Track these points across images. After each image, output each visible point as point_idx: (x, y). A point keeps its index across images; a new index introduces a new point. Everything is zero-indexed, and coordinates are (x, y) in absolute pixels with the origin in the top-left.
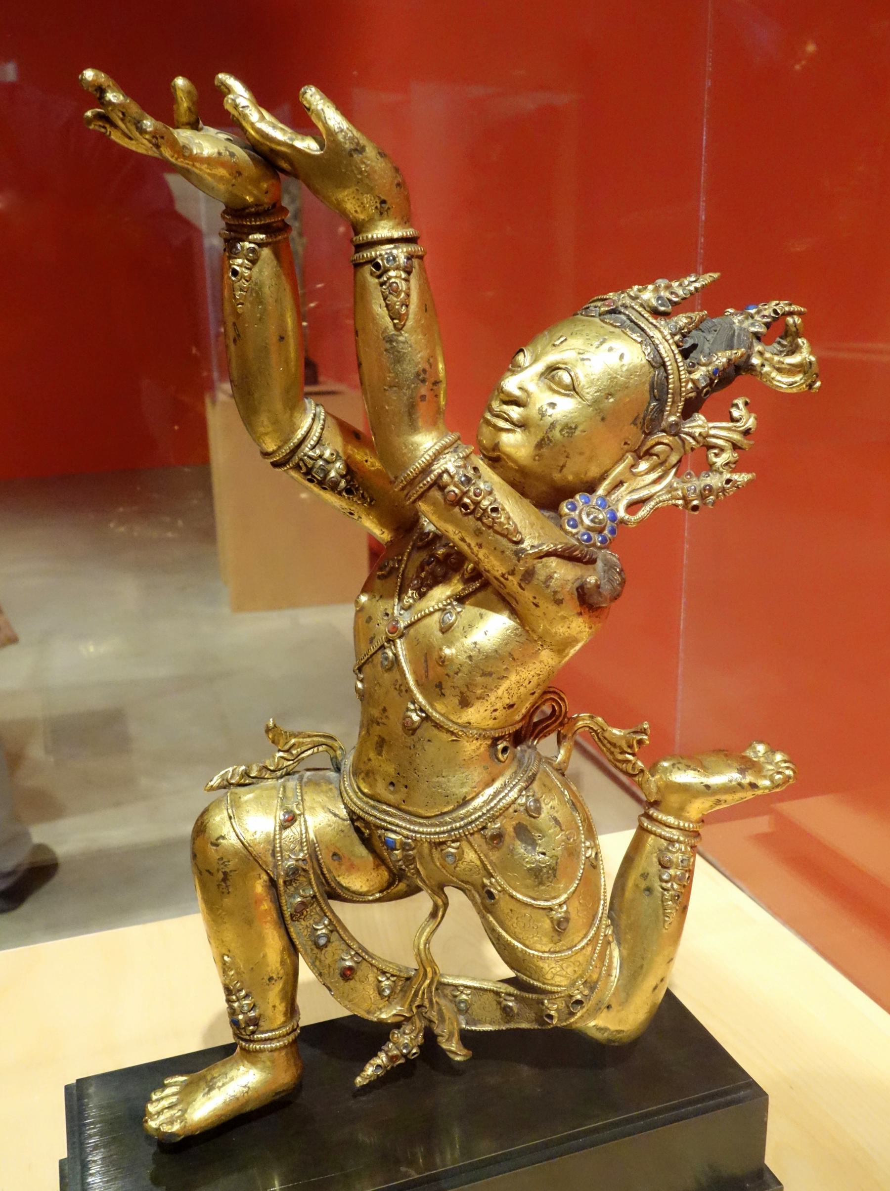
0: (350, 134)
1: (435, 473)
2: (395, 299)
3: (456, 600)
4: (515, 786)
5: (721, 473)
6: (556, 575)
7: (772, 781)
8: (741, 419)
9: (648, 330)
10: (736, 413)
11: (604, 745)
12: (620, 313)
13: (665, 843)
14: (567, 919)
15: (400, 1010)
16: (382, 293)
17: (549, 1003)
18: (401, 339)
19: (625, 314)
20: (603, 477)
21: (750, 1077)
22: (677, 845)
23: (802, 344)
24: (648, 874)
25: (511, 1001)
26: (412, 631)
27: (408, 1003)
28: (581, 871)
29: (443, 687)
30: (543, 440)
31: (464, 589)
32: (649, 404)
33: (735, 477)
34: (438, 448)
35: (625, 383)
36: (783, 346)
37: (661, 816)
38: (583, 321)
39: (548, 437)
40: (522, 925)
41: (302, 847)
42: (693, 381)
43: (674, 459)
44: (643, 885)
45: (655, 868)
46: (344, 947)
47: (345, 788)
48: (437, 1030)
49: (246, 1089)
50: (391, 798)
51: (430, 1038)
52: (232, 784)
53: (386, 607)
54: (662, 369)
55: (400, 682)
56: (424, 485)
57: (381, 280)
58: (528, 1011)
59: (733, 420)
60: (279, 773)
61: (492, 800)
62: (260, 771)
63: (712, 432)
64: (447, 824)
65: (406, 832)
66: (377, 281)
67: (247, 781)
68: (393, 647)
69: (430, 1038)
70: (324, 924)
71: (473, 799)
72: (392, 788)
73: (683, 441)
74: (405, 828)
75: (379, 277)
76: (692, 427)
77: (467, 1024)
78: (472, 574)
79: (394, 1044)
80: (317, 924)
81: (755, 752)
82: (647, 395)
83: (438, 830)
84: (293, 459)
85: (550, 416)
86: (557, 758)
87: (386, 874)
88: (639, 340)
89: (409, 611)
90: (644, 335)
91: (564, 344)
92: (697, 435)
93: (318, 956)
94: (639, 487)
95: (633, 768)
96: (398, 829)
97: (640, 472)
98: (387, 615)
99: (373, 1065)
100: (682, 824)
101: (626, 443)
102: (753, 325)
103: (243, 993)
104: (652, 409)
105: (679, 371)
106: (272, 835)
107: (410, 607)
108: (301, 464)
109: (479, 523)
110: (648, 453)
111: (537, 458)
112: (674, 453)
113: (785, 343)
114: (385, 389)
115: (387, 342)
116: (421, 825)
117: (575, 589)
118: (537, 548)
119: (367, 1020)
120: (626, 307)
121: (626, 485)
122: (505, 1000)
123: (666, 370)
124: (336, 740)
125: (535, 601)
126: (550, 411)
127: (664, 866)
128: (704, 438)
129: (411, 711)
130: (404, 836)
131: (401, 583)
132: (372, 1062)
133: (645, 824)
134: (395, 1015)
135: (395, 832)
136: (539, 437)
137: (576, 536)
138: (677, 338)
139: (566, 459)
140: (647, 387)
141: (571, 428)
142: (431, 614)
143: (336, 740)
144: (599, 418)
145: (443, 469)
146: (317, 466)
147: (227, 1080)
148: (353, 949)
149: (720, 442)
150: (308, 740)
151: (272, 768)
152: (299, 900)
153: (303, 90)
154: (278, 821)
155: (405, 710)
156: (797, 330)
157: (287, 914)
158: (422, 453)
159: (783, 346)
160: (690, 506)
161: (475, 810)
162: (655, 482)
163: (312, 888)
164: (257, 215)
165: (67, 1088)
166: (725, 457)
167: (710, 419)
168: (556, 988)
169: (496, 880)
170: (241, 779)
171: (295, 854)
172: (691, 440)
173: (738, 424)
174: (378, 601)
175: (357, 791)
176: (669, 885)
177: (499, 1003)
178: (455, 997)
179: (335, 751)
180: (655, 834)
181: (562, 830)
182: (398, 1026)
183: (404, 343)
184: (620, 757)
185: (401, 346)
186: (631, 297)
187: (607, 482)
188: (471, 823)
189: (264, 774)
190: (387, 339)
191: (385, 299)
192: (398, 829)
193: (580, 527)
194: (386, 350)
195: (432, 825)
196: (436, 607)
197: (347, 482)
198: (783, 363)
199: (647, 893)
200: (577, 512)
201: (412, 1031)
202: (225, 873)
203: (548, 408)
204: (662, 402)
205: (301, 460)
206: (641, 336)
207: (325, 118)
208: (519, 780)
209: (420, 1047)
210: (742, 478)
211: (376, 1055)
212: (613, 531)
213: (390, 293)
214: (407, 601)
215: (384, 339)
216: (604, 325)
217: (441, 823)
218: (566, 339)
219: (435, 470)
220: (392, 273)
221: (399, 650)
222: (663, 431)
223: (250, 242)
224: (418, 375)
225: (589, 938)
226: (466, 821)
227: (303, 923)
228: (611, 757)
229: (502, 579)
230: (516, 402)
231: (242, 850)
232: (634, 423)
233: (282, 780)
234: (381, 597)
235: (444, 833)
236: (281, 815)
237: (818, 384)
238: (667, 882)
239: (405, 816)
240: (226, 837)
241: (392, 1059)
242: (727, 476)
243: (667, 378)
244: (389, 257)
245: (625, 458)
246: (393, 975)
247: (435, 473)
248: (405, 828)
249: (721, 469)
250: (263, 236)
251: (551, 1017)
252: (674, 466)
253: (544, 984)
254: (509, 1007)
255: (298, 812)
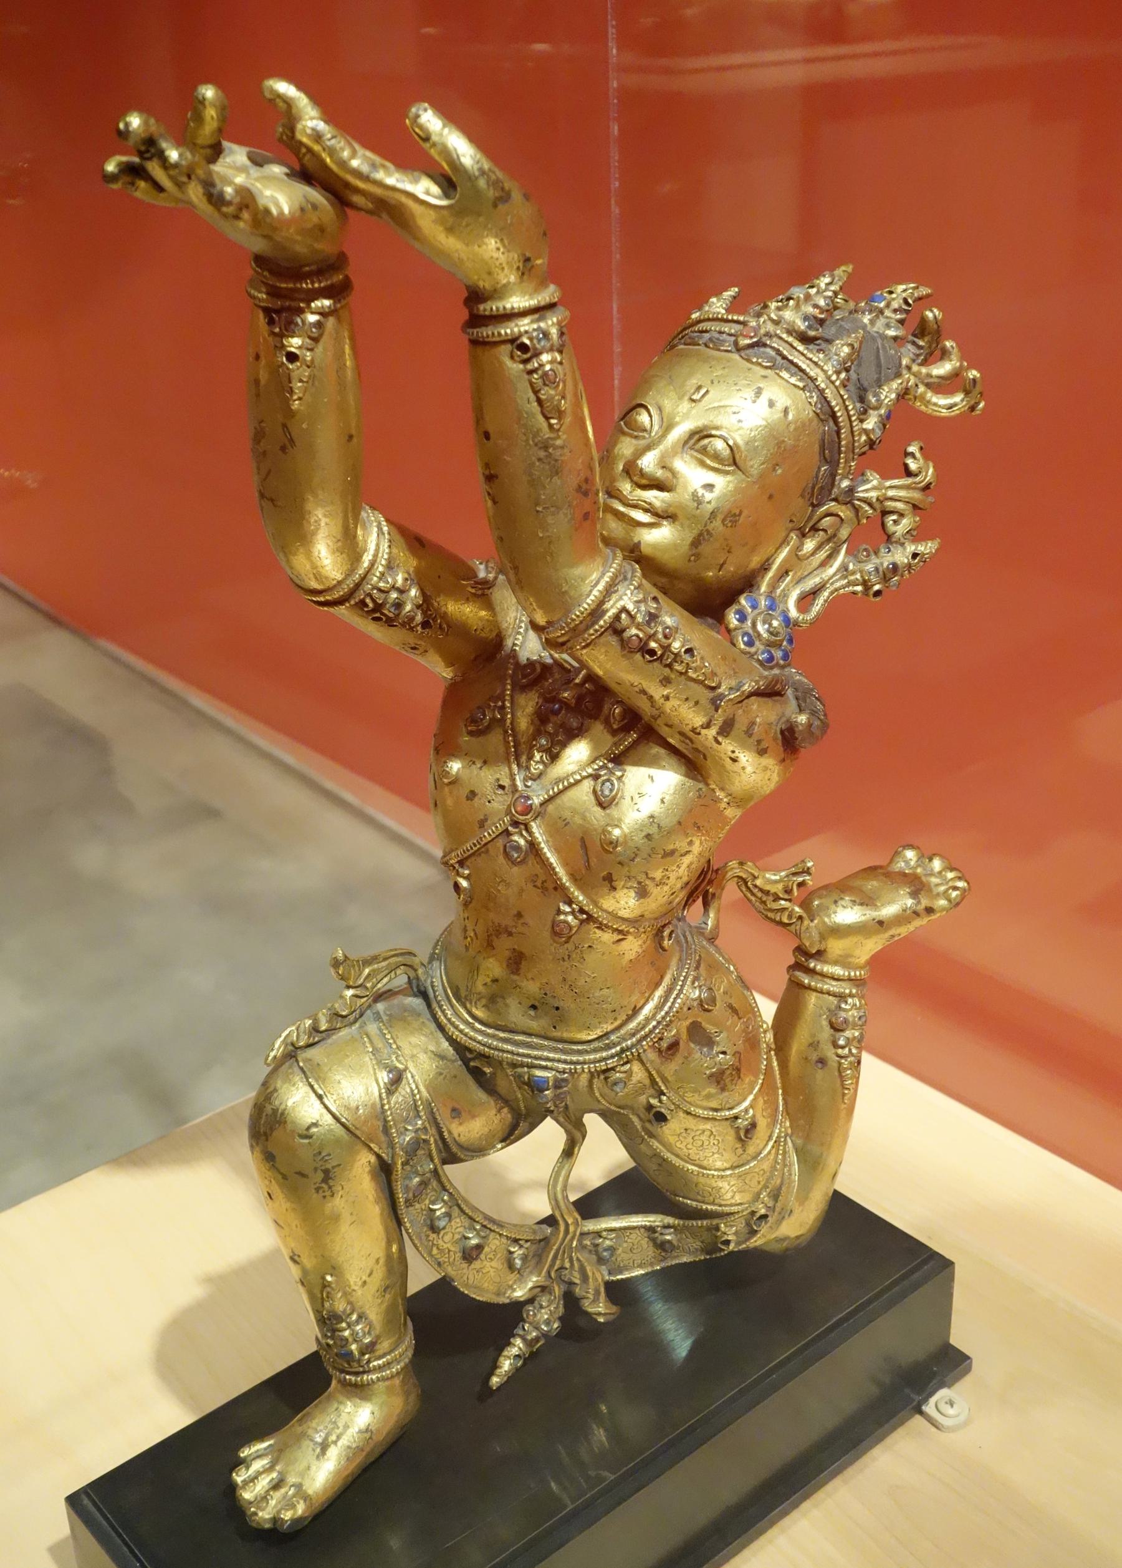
0: (493, 177)
1: (610, 614)
2: (552, 392)
3: (611, 760)
4: (686, 978)
5: (902, 544)
6: (758, 720)
7: (949, 901)
8: (920, 472)
9: (808, 370)
10: (913, 466)
11: (753, 894)
12: (765, 345)
13: (835, 1001)
14: (753, 1125)
15: (537, 1281)
16: (531, 384)
17: (726, 1226)
18: (558, 442)
19: (773, 348)
20: (765, 568)
21: (931, 1249)
22: (850, 1000)
23: (951, 350)
24: (818, 1042)
25: (670, 1234)
26: (551, 808)
27: (545, 1270)
28: (765, 1063)
29: (614, 879)
30: (700, 534)
31: (615, 744)
32: (819, 468)
33: (921, 548)
34: (608, 580)
35: (795, 446)
36: (920, 347)
37: (827, 969)
38: (714, 358)
39: (707, 531)
40: (700, 1143)
41: (418, 1112)
42: (866, 431)
43: (844, 533)
44: (814, 1057)
45: (826, 1033)
46: (467, 1222)
47: (449, 1020)
48: (578, 1291)
49: (368, 1435)
50: (534, 1025)
51: (571, 1301)
52: (300, 1048)
53: (498, 776)
54: (831, 423)
55: (542, 878)
56: (596, 631)
57: (529, 367)
58: (690, 1240)
59: (908, 473)
60: (352, 1018)
61: (666, 1001)
62: (329, 1021)
63: (891, 493)
64: (615, 1045)
65: (561, 1066)
66: (521, 366)
67: (316, 1039)
68: (524, 833)
69: (571, 1301)
70: (443, 1201)
71: (642, 1007)
72: (532, 1013)
73: (857, 510)
74: (559, 1061)
75: (525, 362)
76: (866, 491)
77: (610, 1274)
78: (623, 723)
79: (530, 1323)
80: (433, 1203)
81: (907, 862)
82: (817, 457)
83: (604, 1054)
84: (357, 594)
85: (709, 502)
86: (706, 924)
87: (506, 1115)
88: (801, 385)
89: (538, 782)
90: (804, 376)
91: (706, 398)
92: (874, 500)
93: (435, 1242)
94: (806, 573)
95: (790, 917)
96: (549, 1064)
97: (805, 555)
98: (502, 787)
99: (509, 1358)
100: (852, 974)
101: (791, 521)
102: (888, 326)
103: (354, 1317)
104: (823, 475)
105: (851, 422)
106: (379, 1106)
107: (540, 775)
108: (368, 600)
109: (667, 670)
110: (815, 529)
111: (693, 558)
112: (845, 525)
113: (921, 343)
114: (538, 511)
115: (540, 448)
116: (579, 1052)
117: (779, 732)
118: (738, 690)
119: (498, 1305)
120: (771, 337)
121: (791, 574)
122: (662, 1234)
123: (836, 422)
124: (415, 956)
125: (733, 756)
126: (708, 496)
127: (836, 1028)
128: (881, 502)
129: (566, 914)
130: (557, 1071)
131: (514, 741)
132: (505, 1353)
133: (806, 981)
134: (531, 1289)
135: (546, 1068)
136: (696, 532)
137: (755, 657)
138: (843, 375)
139: (728, 554)
140: (816, 448)
141: (735, 515)
142: (577, 782)
143: (415, 956)
144: (765, 497)
145: (619, 607)
146: (391, 601)
147: (341, 1430)
148: (478, 1222)
149: (900, 506)
150: (384, 964)
151: (344, 1013)
152: (417, 1179)
153: (414, 110)
154: (382, 1085)
155: (555, 912)
156: (939, 327)
157: (401, 1197)
158: (589, 589)
159: (920, 347)
160: (871, 592)
161: (648, 1020)
162: (824, 564)
163: (432, 1160)
164: (320, 273)
165: (73, 1500)
166: (906, 524)
167: (885, 476)
168: (736, 1208)
169: (668, 1098)
170: (309, 1038)
171: (410, 1124)
172: (867, 508)
173: (918, 479)
174: (481, 768)
175: (470, 1020)
176: (846, 1051)
177: (654, 1240)
178: (597, 1245)
179: (416, 970)
180: (815, 990)
181: (740, 1018)
182: (531, 1301)
183: (562, 447)
184: (775, 906)
185: (558, 452)
186: (773, 321)
187: (770, 574)
188: (644, 1038)
189: (334, 1024)
190: (540, 445)
191: (536, 392)
192: (549, 1064)
193: (757, 643)
194: (539, 460)
195: (595, 1051)
196: (584, 774)
197: (424, 613)
198: (932, 377)
199: (820, 1065)
200: (749, 623)
201: (550, 1302)
202: (326, 1172)
203: (704, 491)
204: (834, 464)
205: (370, 595)
206: (801, 380)
207: (458, 156)
208: (688, 969)
209: (560, 1319)
210: (927, 548)
211: (509, 1344)
212: (790, 641)
213: (545, 384)
214: (535, 768)
215: (536, 445)
216: (750, 366)
217: (607, 1045)
218: (707, 392)
219: (607, 611)
220: (545, 357)
221: (537, 835)
222: (835, 500)
223: (312, 313)
224: (579, 489)
225: (774, 1139)
226: (638, 1036)
227: (417, 1206)
228: (761, 907)
229: (691, 734)
230: (660, 486)
231: (346, 1136)
232: (802, 496)
233: (357, 1025)
234: (485, 762)
235: (612, 1057)
236: (384, 1077)
237: (982, 405)
238: (843, 1047)
239: (554, 1044)
240: (320, 1123)
241: (529, 1343)
242: (911, 548)
243: (838, 433)
244: (539, 335)
245: (789, 539)
246: (527, 1241)
247: (610, 614)
248: (559, 1061)
249: (902, 540)
250: (327, 303)
251: (727, 1243)
252: (844, 542)
253: (720, 1206)
254: (669, 1242)
255: (401, 1066)
